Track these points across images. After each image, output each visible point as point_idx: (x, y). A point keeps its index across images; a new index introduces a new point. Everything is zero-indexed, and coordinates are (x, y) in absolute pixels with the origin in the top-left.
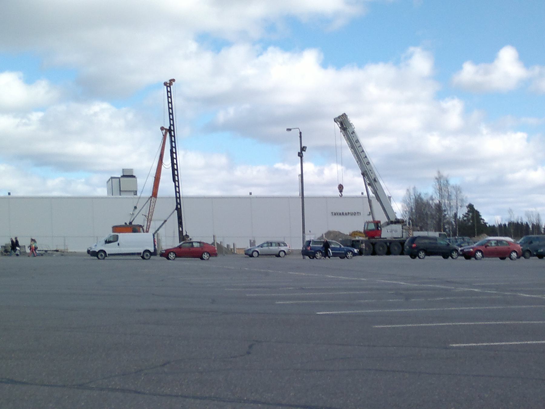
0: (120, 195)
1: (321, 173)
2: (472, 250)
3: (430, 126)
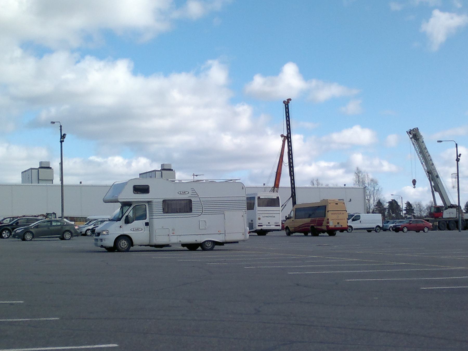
0: (38, 183)
1: (129, 164)
2: (400, 227)
3: (224, 127)
